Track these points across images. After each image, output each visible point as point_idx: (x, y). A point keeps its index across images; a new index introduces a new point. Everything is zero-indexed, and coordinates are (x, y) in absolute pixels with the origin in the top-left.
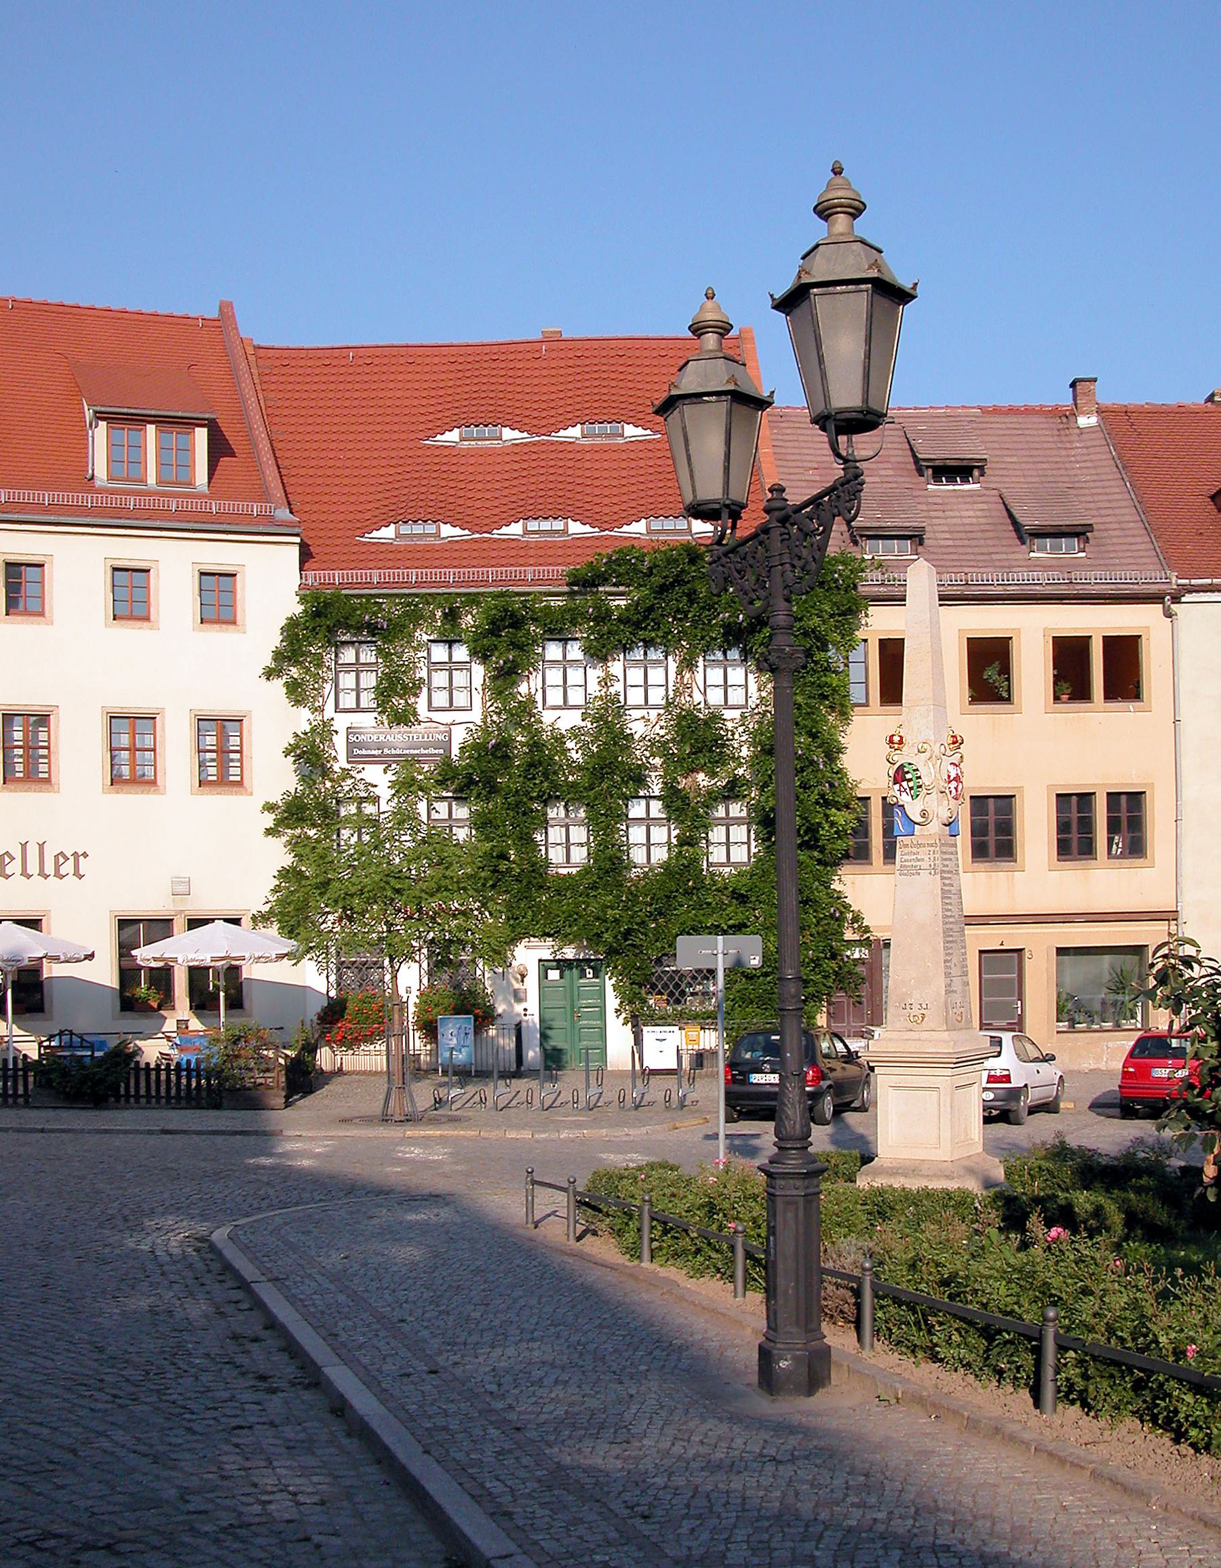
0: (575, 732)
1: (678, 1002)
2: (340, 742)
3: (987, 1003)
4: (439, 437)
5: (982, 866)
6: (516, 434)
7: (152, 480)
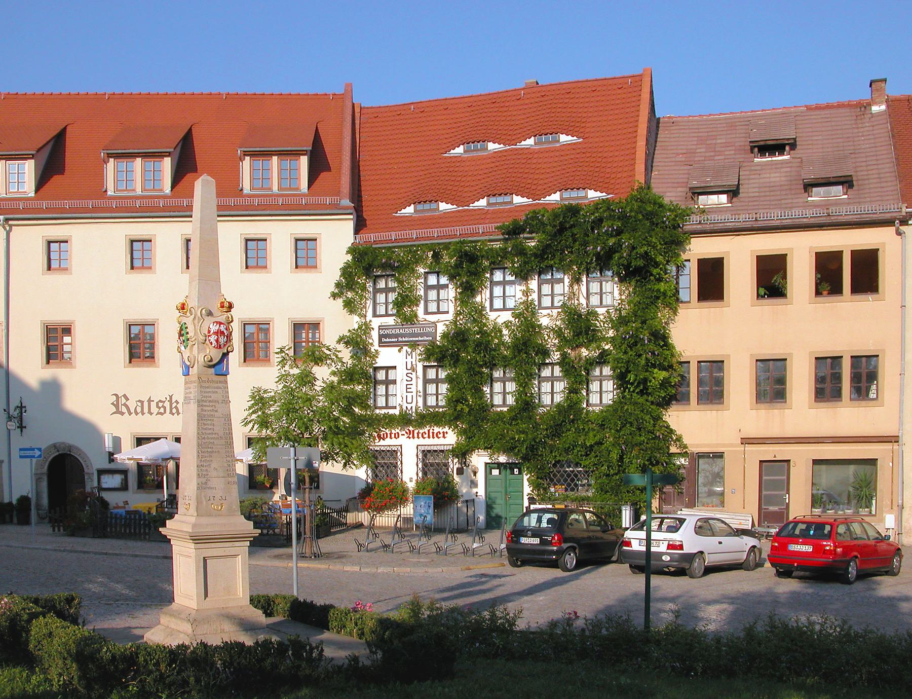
0: (507, 324)
1: (572, 490)
2: (375, 335)
3: (765, 496)
4: (452, 151)
5: (762, 406)
6: (497, 146)
7: (275, 188)
